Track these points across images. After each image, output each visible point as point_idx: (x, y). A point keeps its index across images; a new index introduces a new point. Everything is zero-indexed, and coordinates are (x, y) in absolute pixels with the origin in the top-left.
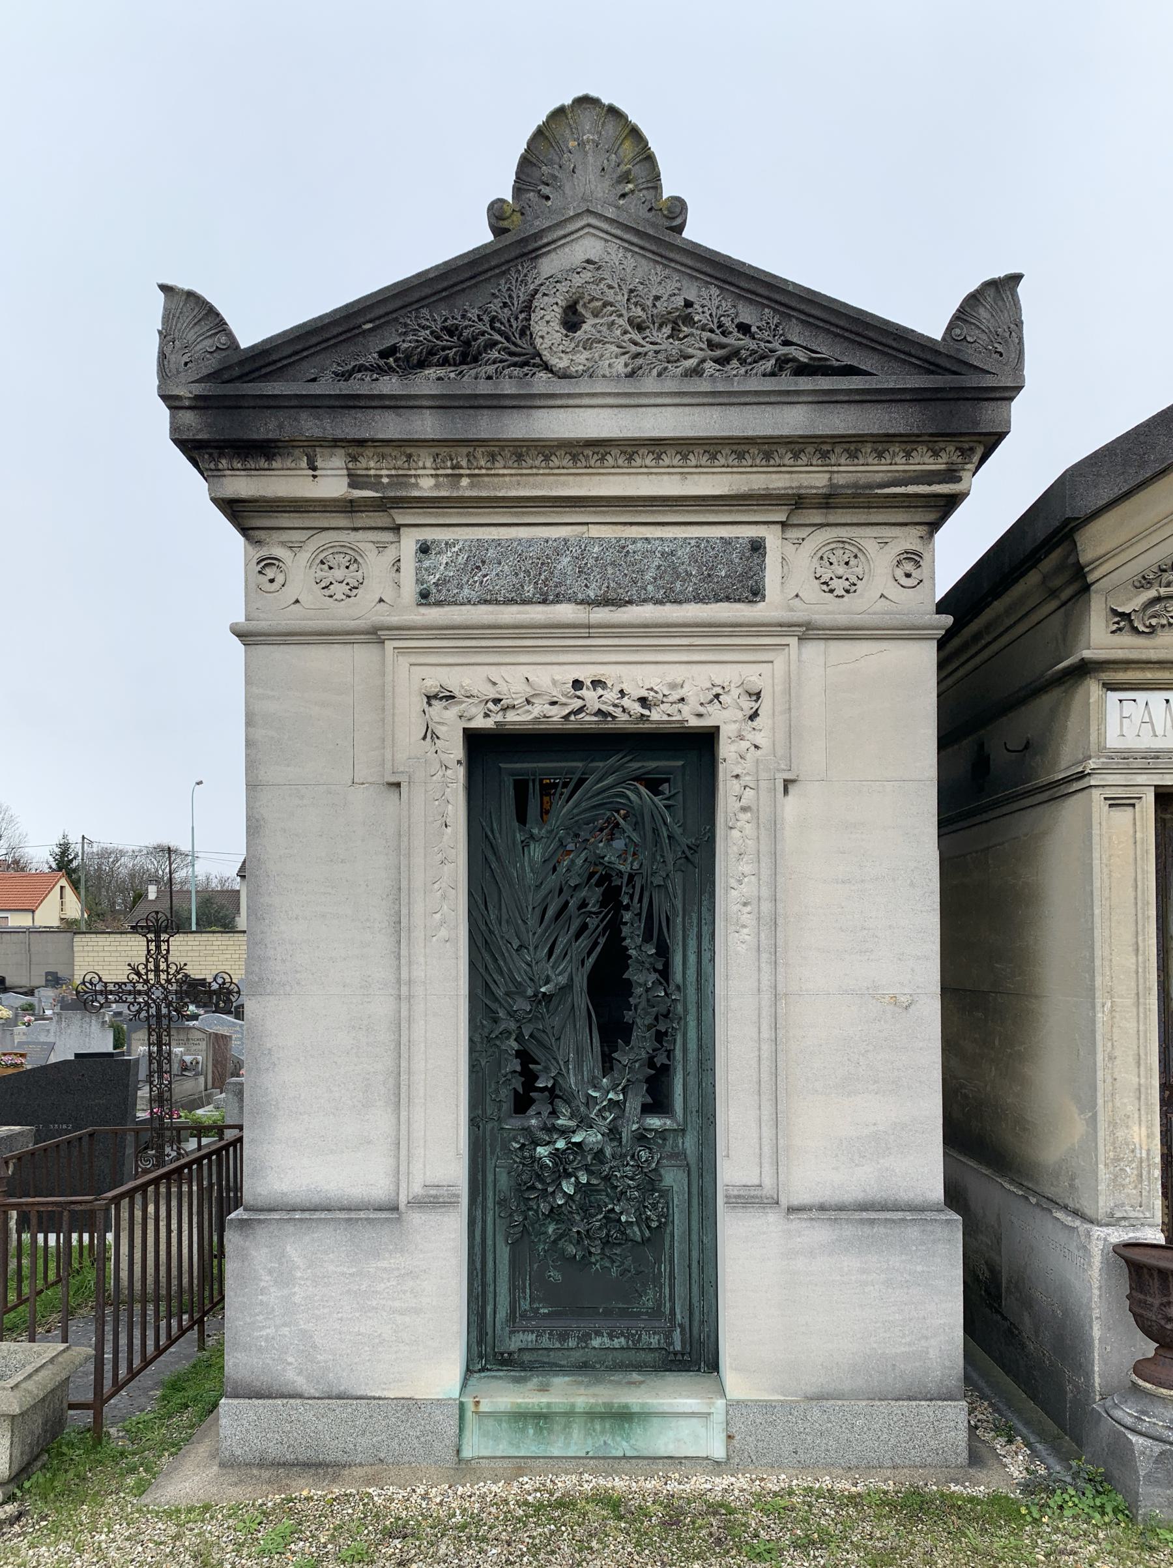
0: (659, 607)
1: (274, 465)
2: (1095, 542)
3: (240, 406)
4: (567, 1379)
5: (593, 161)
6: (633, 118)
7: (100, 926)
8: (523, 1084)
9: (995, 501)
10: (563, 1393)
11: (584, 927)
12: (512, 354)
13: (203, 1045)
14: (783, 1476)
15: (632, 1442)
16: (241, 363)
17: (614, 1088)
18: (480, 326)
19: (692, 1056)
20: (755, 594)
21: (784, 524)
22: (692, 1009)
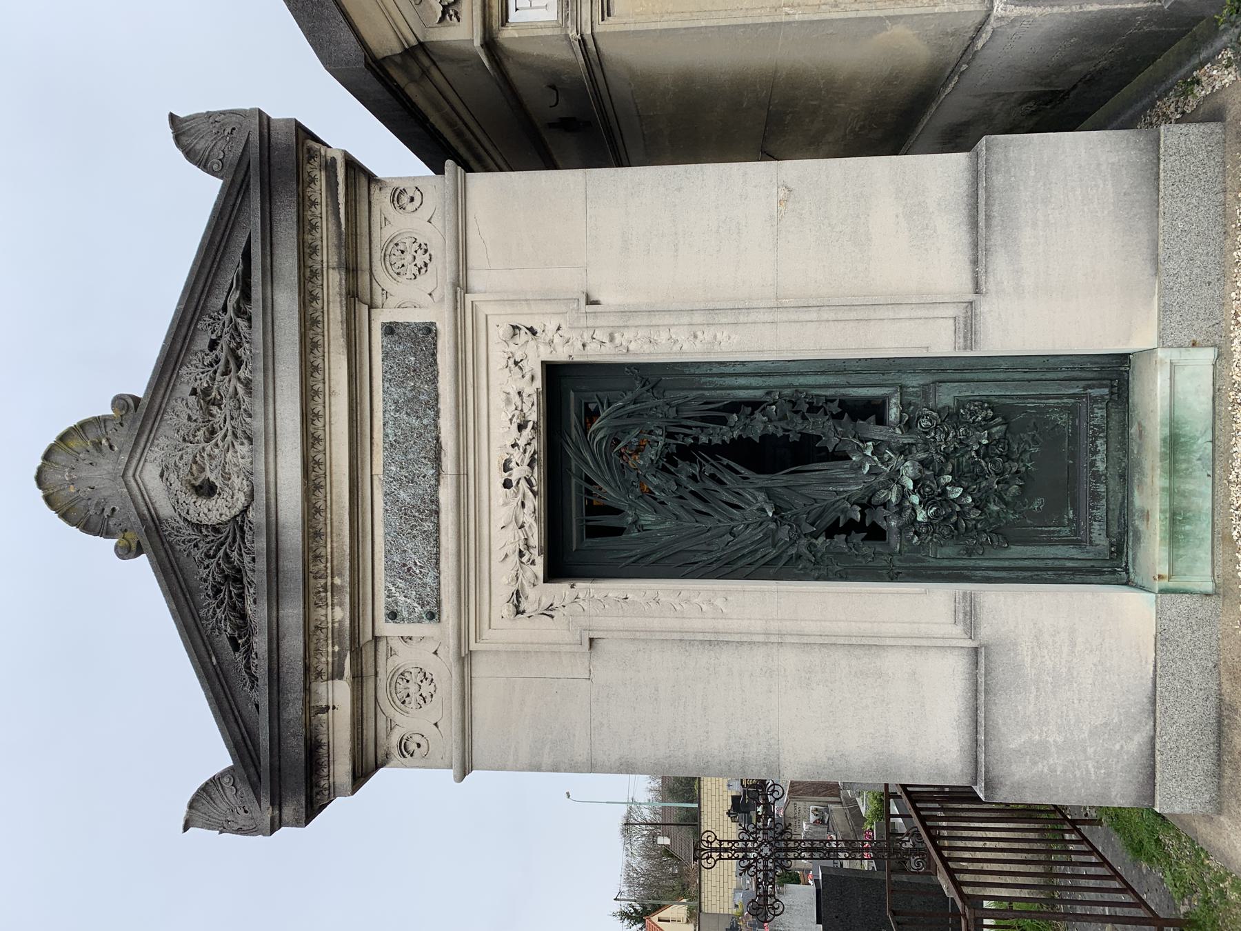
0: (442, 414)
1: (325, 741)
2: (385, 42)
3: (280, 769)
4: (1136, 493)
5: (85, 472)
6: (52, 439)
7: (693, 888)
8: (857, 532)
9: (353, 130)
10: (1151, 496)
11: (713, 477)
12: (234, 541)
13: (800, 804)
14: (1233, 294)
15: (1198, 434)
16: (245, 767)
17: (861, 450)
18: (213, 567)
19: (832, 380)
20: (430, 331)
21: (371, 307)
22: (789, 380)
